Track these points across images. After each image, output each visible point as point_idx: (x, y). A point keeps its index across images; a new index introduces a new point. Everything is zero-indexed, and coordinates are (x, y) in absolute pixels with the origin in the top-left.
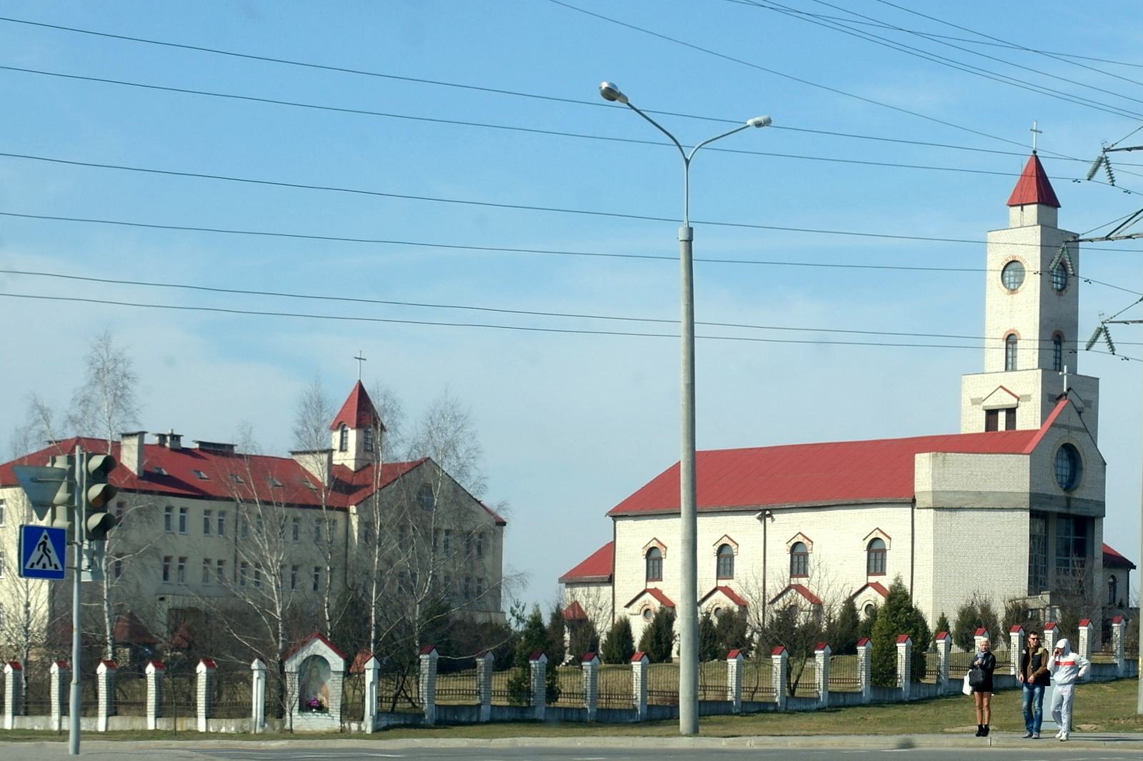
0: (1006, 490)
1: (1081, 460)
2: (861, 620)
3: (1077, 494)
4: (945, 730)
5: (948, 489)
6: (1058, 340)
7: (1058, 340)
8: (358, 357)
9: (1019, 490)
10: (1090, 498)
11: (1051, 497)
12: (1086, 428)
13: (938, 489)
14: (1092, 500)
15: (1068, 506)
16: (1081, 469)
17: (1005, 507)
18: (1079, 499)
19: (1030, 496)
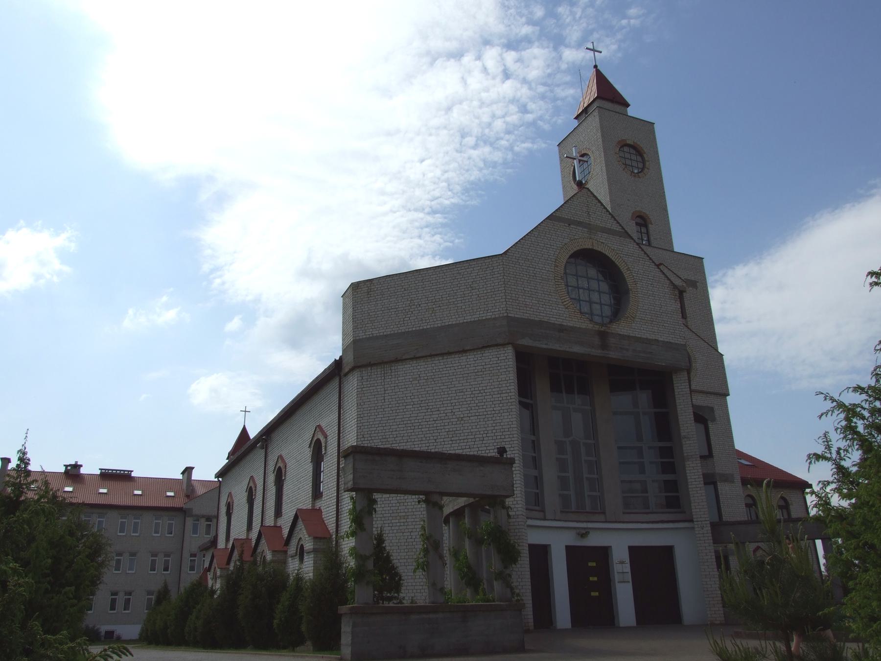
0: (469, 318)
1: (624, 279)
2: (592, 593)
3: (621, 328)
4: (850, 637)
5: (375, 333)
6: (750, 501)
7: (750, 501)
8: (621, 571)
9: (489, 315)
10: (653, 337)
11: (561, 329)
12: (626, 232)
13: (362, 335)
14: (657, 341)
15: (604, 346)
16: (627, 292)
17: (466, 348)
18: (623, 337)
19: (711, 525)
